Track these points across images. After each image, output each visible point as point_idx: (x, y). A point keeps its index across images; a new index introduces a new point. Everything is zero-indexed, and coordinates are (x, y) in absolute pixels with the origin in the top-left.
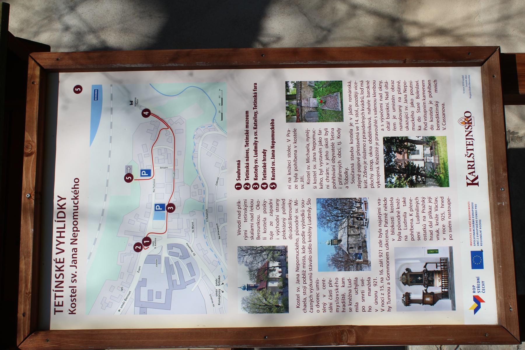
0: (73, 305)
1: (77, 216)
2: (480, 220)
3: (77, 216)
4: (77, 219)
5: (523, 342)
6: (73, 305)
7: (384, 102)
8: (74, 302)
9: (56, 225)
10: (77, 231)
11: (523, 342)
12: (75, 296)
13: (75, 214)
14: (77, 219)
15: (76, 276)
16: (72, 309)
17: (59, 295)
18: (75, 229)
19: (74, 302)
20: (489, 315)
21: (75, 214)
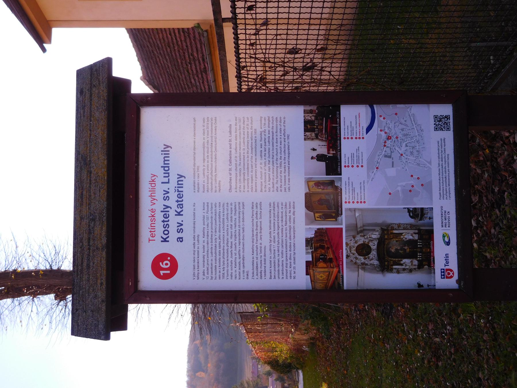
0: (166, 232)
1: (169, 160)
2: (448, 155)
3: (169, 160)
4: (164, 173)
5: (112, 334)
6: (166, 232)
7: (230, 223)
8: (166, 229)
9: (105, 135)
10: (164, 167)
11: (112, 334)
12: (168, 221)
13: (166, 159)
14: (164, 173)
15: (182, 225)
16: (165, 237)
17: (144, 307)
18: (153, 185)
19: (166, 229)
20: (452, 283)
21: (166, 159)
